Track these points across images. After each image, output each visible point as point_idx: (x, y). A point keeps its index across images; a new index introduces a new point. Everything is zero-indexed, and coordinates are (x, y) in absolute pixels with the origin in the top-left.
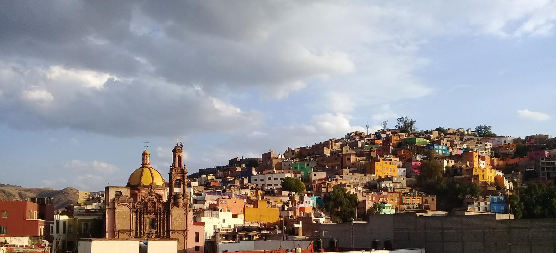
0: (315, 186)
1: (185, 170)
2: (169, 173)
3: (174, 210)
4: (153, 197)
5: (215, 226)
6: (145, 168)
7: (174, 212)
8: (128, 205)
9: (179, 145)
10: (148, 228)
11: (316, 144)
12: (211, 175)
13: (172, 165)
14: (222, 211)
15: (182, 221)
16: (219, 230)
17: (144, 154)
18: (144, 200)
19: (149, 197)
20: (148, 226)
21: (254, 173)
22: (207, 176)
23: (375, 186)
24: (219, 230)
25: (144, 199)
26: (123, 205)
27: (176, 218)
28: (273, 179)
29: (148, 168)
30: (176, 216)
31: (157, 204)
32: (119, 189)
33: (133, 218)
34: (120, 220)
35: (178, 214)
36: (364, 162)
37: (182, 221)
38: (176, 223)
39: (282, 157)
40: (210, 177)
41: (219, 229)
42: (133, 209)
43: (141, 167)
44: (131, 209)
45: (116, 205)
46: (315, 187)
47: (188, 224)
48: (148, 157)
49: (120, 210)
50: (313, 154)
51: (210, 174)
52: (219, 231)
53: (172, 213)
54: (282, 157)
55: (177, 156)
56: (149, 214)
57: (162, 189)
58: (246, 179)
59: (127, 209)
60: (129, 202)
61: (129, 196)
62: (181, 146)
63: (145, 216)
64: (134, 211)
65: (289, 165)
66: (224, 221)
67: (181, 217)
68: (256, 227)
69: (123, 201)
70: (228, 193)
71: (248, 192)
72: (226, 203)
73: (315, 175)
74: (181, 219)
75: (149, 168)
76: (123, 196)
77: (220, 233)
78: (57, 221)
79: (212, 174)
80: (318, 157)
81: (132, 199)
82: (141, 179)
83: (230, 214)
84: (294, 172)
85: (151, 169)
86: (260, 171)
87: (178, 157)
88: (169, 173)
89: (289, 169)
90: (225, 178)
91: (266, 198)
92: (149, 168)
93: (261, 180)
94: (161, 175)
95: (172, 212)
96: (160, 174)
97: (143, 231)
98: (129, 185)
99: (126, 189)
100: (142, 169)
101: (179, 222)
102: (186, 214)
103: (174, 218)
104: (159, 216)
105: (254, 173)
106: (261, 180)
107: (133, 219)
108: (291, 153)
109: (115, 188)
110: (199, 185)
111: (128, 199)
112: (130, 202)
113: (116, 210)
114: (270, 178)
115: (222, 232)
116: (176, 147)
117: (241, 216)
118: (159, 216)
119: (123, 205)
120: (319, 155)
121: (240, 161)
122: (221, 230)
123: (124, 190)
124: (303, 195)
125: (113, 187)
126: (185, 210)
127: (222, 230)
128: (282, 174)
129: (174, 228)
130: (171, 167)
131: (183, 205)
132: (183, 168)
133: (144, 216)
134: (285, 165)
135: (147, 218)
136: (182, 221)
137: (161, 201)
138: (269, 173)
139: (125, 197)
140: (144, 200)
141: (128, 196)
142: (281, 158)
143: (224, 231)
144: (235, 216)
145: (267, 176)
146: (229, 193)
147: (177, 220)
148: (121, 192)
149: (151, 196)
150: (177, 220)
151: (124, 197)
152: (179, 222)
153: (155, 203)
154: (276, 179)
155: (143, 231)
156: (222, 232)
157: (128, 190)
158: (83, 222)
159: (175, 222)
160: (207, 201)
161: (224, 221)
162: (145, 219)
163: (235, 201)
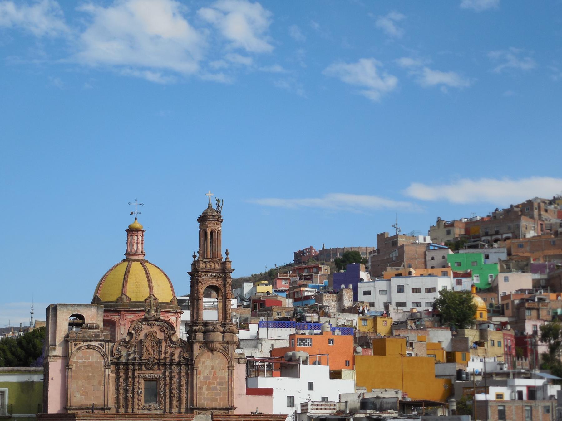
0: (507, 304)
3: (202, 359)
4: (155, 329)
5: (292, 398)
6: (133, 263)
7: (204, 363)
8: (98, 347)
9: (214, 207)
10: (143, 404)
11: (497, 210)
12: (264, 284)
13: (198, 253)
14: (306, 364)
15: (220, 384)
16: (305, 408)
17: (131, 231)
18: (135, 335)
19: (146, 329)
20: (143, 396)
21: (364, 275)
22: (255, 286)
23: (126, 364)
24: (305, 408)
25: (133, 332)
26: (89, 347)
27: (206, 378)
28: (408, 290)
30: (206, 372)
33: (110, 378)
35: (212, 369)
38: (208, 389)
39: (425, 240)
40: (263, 289)
41: (307, 405)
42: (109, 357)
43: (124, 261)
44: (104, 356)
45: (73, 349)
46: (507, 308)
47: (236, 392)
48: (140, 238)
49: (81, 358)
50: (497, 233)
51: (262, 282)
52: (307, 409)
53: (199, 365)
54: (425, 240)
55: (209, 232)
57: (171, 310)
58: (348, 290)
59: (95, 357)
60: (101, 341)
61: (101, 325)
63: (136, 374)
64: (111, 360)
65: (444, 257)
66: (311, 386)
67: (219, 375)
68: (394, 400)
70: (311, 322)
71: (355, 319)
72: (311, 346)
73: (506, 279)
74: (218, 380)
75: (142, 262)
77: (308, 414)
78: (487, 255)
79: (266, 282)
80: (508, 238)
81: (107, 333)
82: (124, 287)
83: (325, 370)
84: (456, 275)
86: (376, 274)
89: (444, 267)
90: (295, 290)
91: (397, 334)
92: (142, 262)
95: (199, 362)
97: (133, 409)
98: (96, 301)
99: (94, 310)
102: (230, 368)
103: (202, 377)
104: (168, 374)
105: (364, 275)
107: (110, 380)
108: (443, 231)
110: (238, 306)
112: (103, 341)
113: (73, 359)
114: (401, 289)
115: (314, 411)
117: (349, 375)
118: (168, 374)
119: (89, 347)
120: (510, 235)
121: (318, 254)
122: (309, 407)
124: (484, 327)
125: (66, 305)
127: (314, 407)
128: (429, 278)
129: (202, 401)
130: (194, 257)
131: (223, 346)
132: (224, 260)
133: (133, 373)
134: (433, 259)
135: (141, 379)
136: (220, 384)
137: (174, 339)
138: (398, 275)
139: (92, 329)
140: (135, 335)
141: (97, 327)
142: (423, 242)
143: (317, 409)
144: (336, 375)
145: (396, 282)
146: (314, 322)
147: (210, 384)
148: (81, 317)
149: (149, 327)
150: (210, 384)
151: (89, 328)
152: (215, 389)
153: (160, 342)
154: (416, 290)
155: (133, 409)
156: (314, 411)
158: (7, 389)
159: (204, 388)
160: (264, 342)
161: (311, 386)
162: (136, 380)
163: (332, 340)
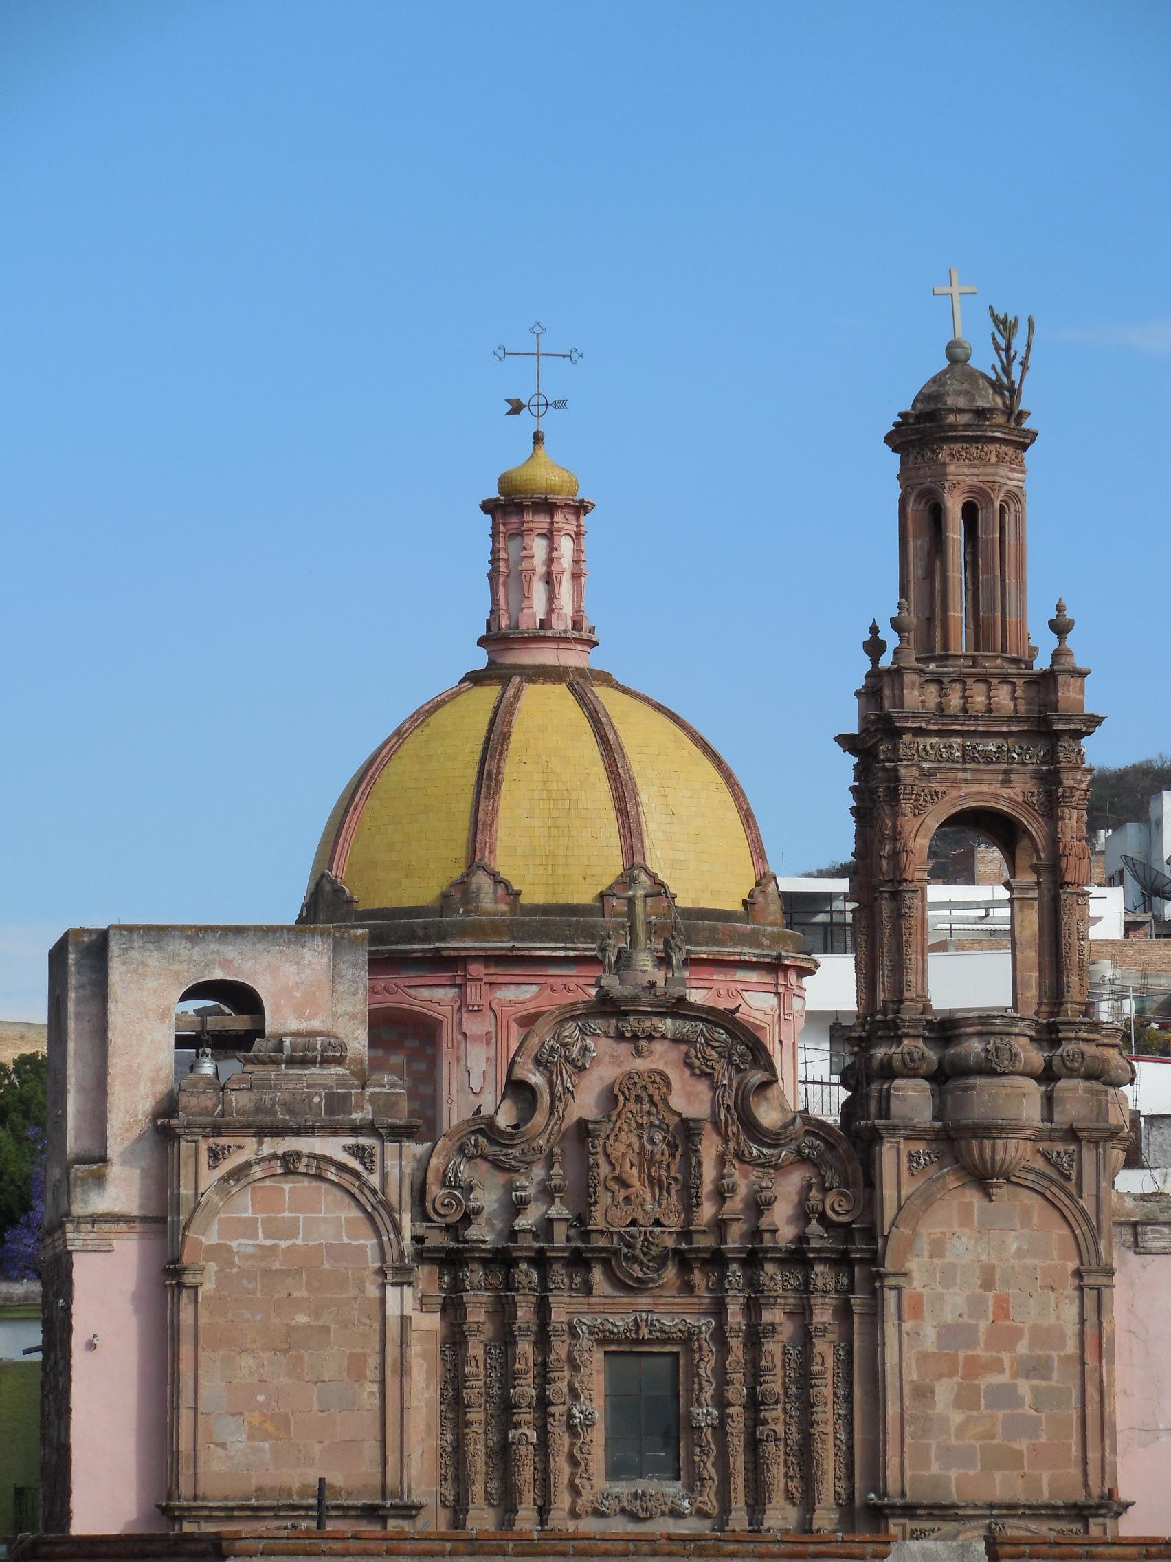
1: (1067, 692)
2: (853, 728)
3: (929, 1230)
4: (661, 1058)
7: (938, 1249)
8: (342, 1167)
9: (984, 360)
13: (896, 624)
15: (1036, 1368)
25: (536, 1078)
26: (289, 1163)
27: (951, 1334)
29: (562, 689)
31: (709, 1148)
32: (226, 964)
33: (413, 1337)
34: (247, 1362)
35: (988, 1284)
36: (242, 1446)
37: (1045, 1377)
42: (406, 1220)
43: (475, 678)
49: (247, 1228)
53: (913, 1265)
56: (620, 1284)
60: (355, 1130)
61: (357, 1041)
62: (1007, 371)
63: (558, 1316)
64: (418, 1239)
67: (1027, 1315)
69: (281, 1116)
74: (1023, 1348)
76: (279, 1048)
85: (603, 694)
87: (970, 512)
88: (853, 728)
93: (320, 1479)
94: (747, 817)
95: (909, 1246)
96: (747, 817)
100: (488, 695)
101: (993, 1391)
103: (930, 1333)
104: (735, 1316)
106: (320, 1479)
107: (414, 1350)
109: (177, 946)
111: (342, 1081)
112: (371, 1129)
116: (938, 380)
118: (735, 1316)
119: (289, 1163)
123: (289, 971)
125: (157, 933)
126: (1082, 1229)
129: (935, 1469)
130: (874, 647)
132: (1042, 663)
133: (543, 1309)
136: (1036, 1368)
137: (768, 1116)
139: (304, 1062)
141: (334, 1055)
147: (974, 1367)
149: (624, 1048)
150: (974, 1367)
151: (291, 1062)
153: (687, 1132)
157: (335, 977)
159: (944, 1391)
162: (560, 1347)
